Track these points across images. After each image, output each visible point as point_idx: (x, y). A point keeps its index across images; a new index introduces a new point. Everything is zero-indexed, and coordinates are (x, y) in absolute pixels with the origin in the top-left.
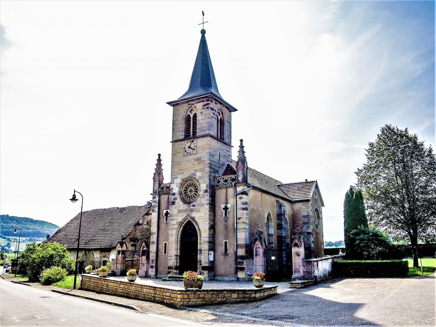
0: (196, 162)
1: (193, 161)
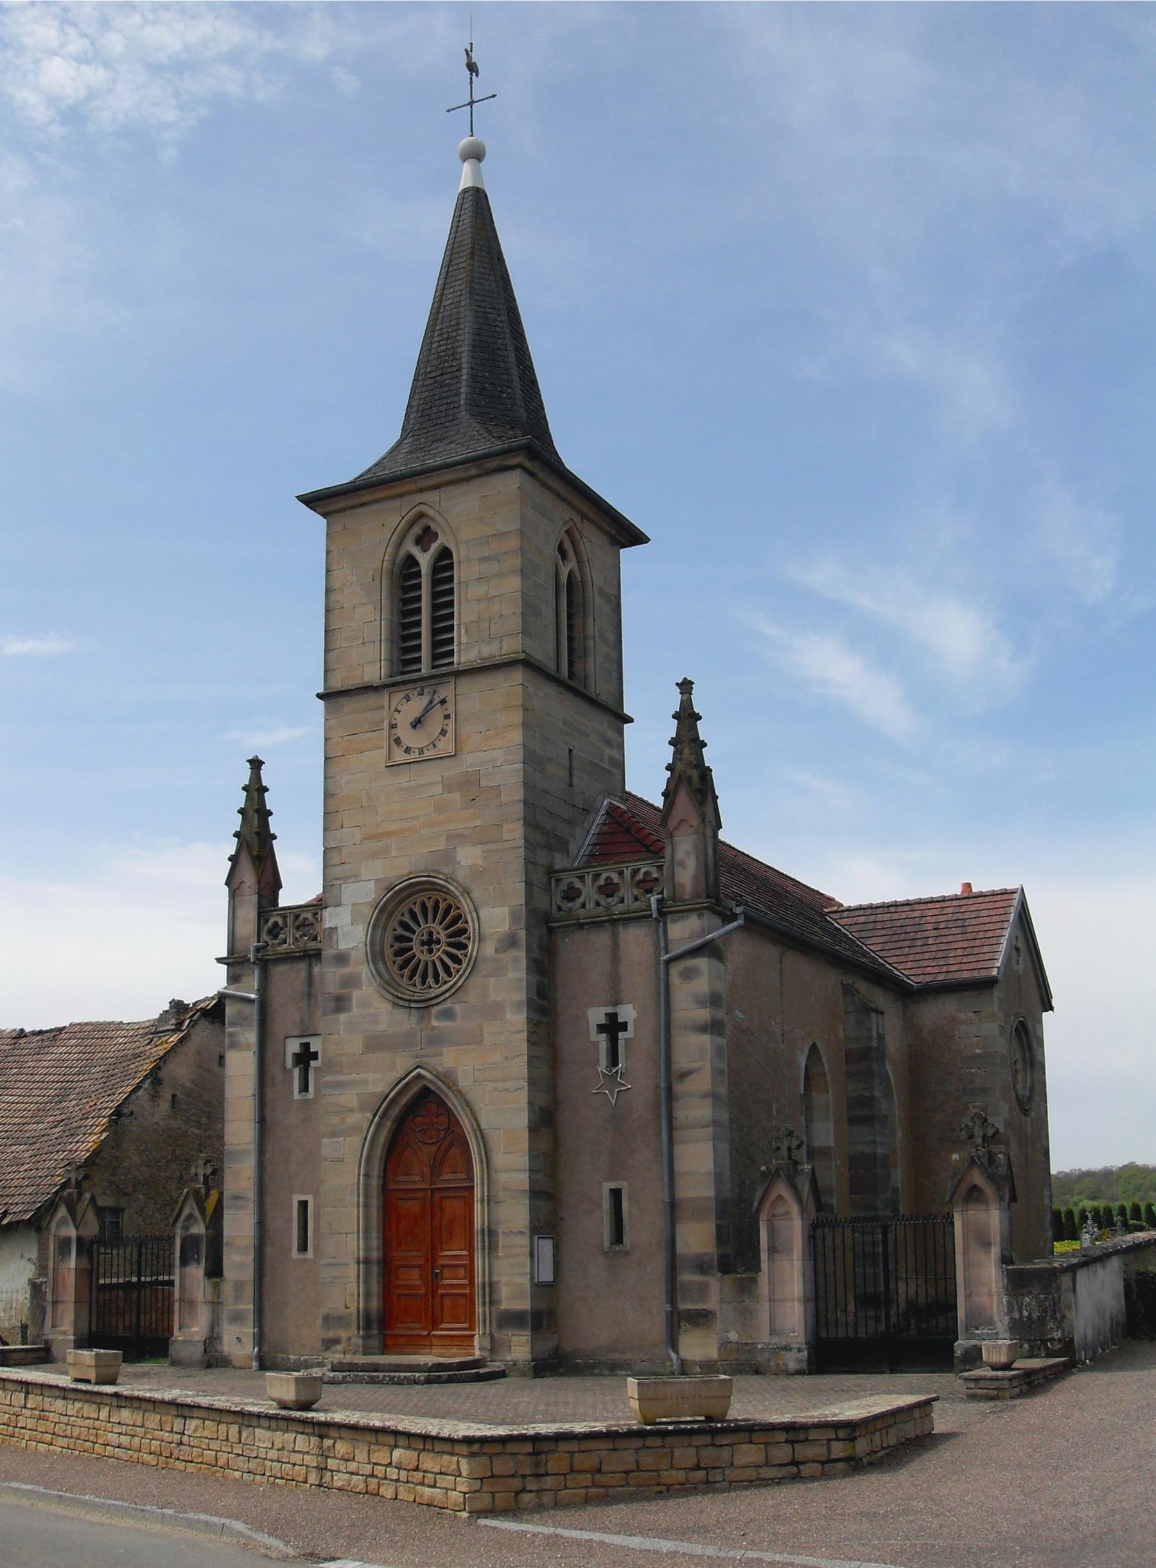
0: (456, 796)
1: (438, 789)
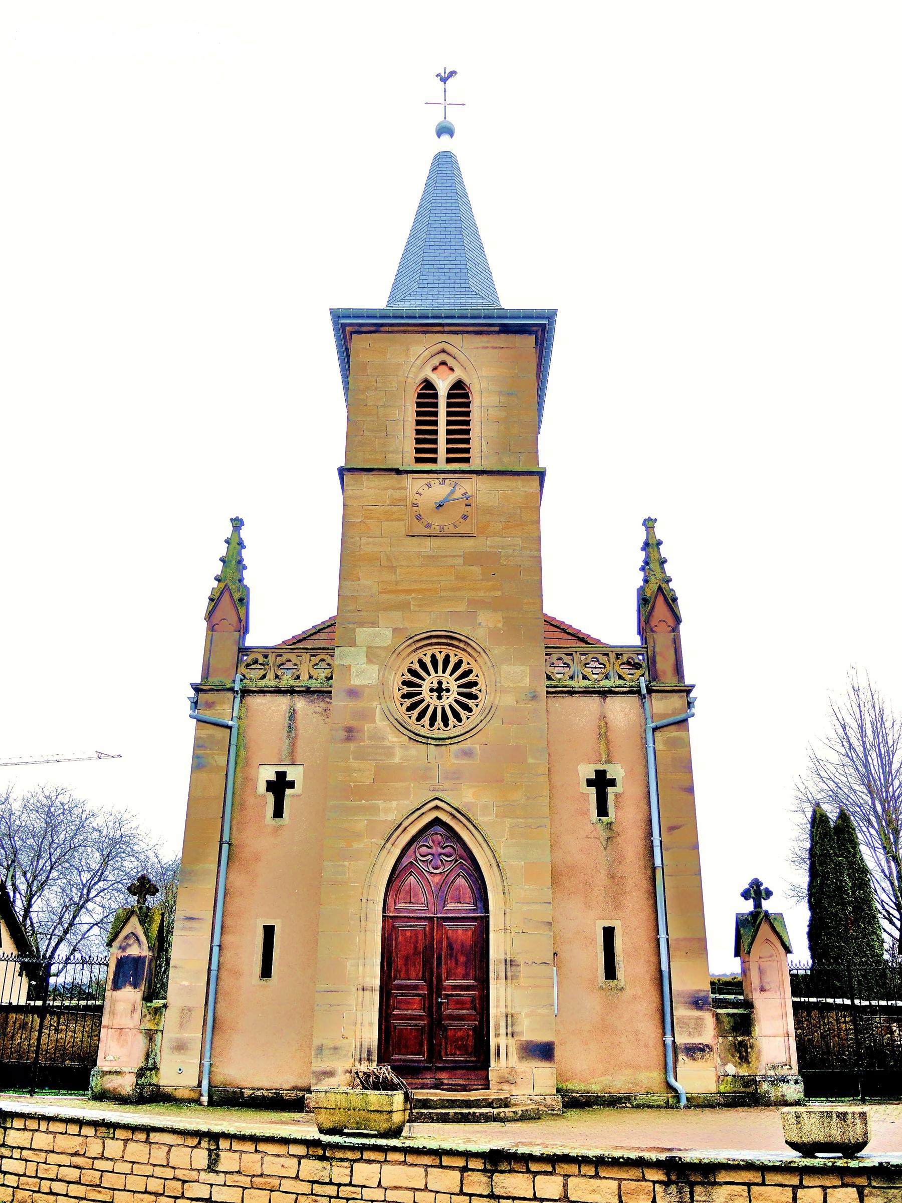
0: (476, 569)
